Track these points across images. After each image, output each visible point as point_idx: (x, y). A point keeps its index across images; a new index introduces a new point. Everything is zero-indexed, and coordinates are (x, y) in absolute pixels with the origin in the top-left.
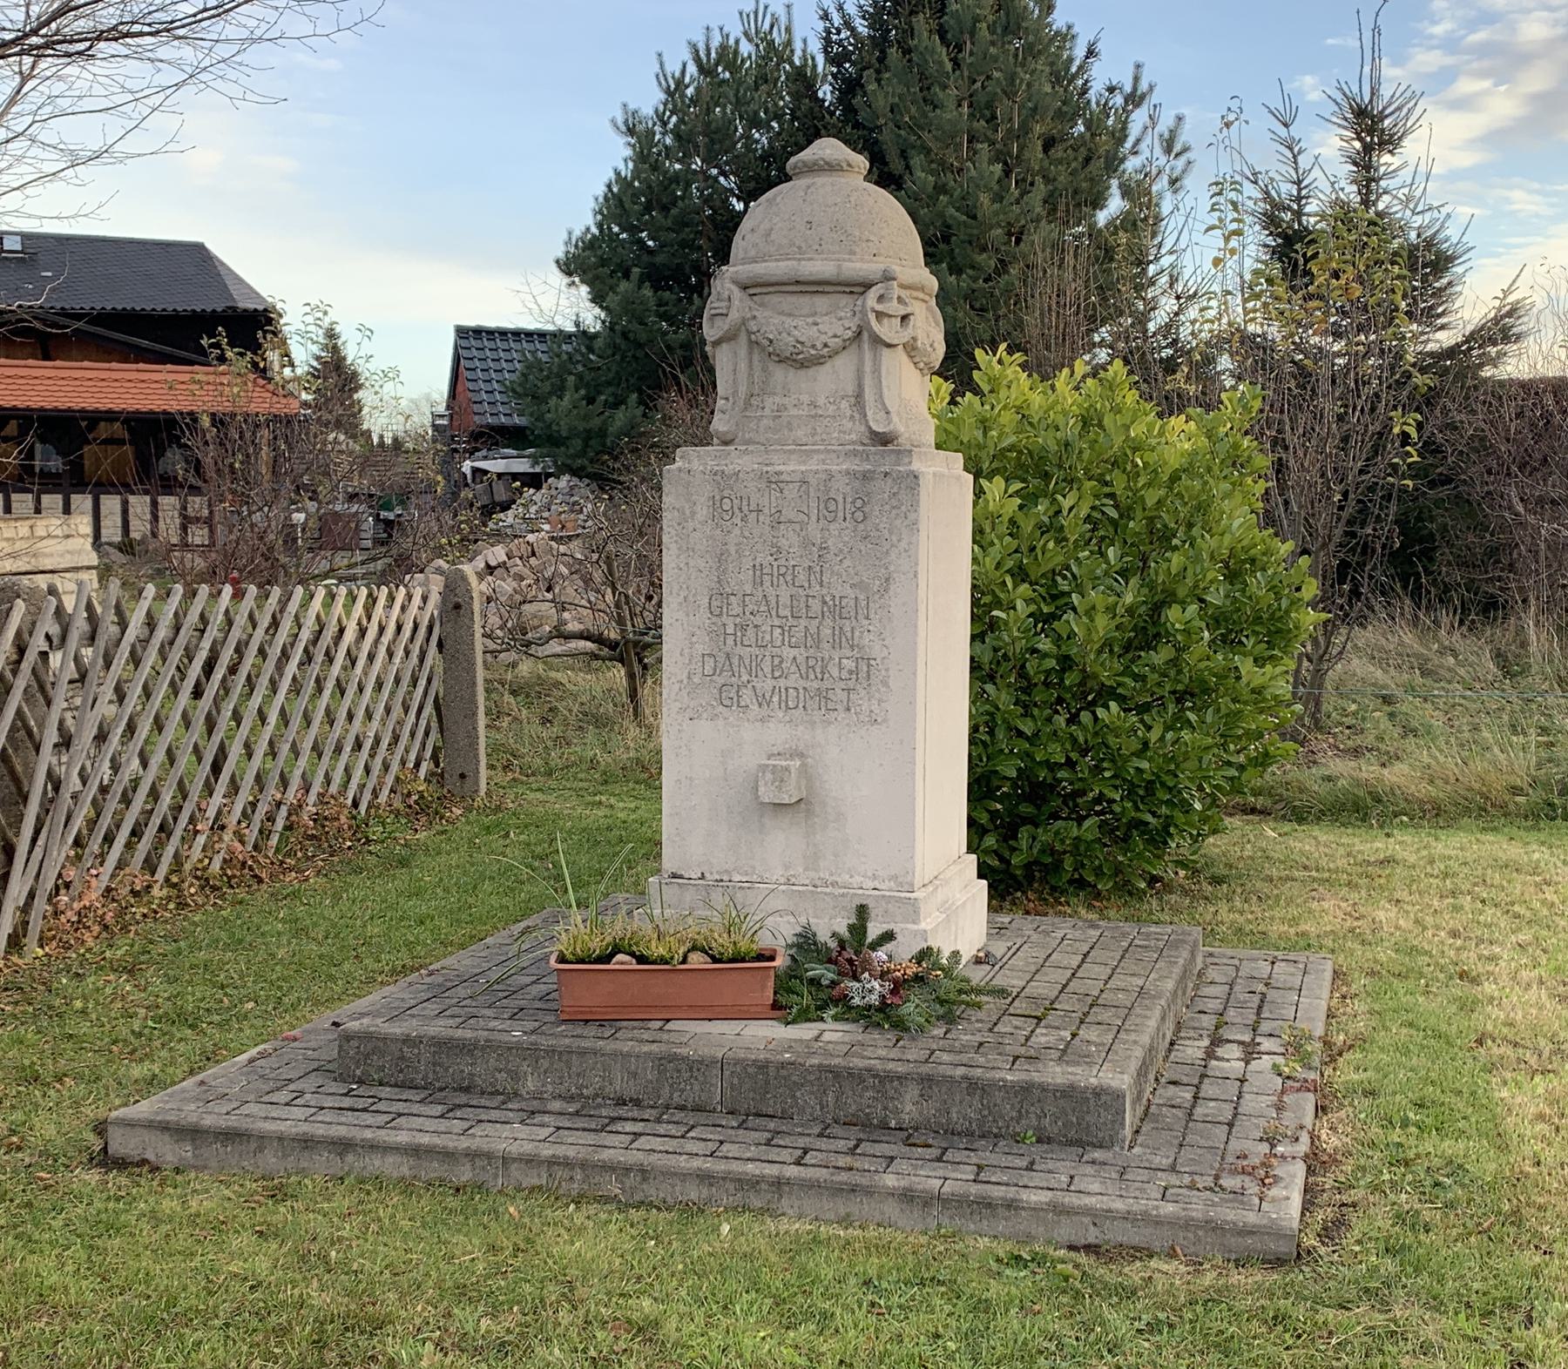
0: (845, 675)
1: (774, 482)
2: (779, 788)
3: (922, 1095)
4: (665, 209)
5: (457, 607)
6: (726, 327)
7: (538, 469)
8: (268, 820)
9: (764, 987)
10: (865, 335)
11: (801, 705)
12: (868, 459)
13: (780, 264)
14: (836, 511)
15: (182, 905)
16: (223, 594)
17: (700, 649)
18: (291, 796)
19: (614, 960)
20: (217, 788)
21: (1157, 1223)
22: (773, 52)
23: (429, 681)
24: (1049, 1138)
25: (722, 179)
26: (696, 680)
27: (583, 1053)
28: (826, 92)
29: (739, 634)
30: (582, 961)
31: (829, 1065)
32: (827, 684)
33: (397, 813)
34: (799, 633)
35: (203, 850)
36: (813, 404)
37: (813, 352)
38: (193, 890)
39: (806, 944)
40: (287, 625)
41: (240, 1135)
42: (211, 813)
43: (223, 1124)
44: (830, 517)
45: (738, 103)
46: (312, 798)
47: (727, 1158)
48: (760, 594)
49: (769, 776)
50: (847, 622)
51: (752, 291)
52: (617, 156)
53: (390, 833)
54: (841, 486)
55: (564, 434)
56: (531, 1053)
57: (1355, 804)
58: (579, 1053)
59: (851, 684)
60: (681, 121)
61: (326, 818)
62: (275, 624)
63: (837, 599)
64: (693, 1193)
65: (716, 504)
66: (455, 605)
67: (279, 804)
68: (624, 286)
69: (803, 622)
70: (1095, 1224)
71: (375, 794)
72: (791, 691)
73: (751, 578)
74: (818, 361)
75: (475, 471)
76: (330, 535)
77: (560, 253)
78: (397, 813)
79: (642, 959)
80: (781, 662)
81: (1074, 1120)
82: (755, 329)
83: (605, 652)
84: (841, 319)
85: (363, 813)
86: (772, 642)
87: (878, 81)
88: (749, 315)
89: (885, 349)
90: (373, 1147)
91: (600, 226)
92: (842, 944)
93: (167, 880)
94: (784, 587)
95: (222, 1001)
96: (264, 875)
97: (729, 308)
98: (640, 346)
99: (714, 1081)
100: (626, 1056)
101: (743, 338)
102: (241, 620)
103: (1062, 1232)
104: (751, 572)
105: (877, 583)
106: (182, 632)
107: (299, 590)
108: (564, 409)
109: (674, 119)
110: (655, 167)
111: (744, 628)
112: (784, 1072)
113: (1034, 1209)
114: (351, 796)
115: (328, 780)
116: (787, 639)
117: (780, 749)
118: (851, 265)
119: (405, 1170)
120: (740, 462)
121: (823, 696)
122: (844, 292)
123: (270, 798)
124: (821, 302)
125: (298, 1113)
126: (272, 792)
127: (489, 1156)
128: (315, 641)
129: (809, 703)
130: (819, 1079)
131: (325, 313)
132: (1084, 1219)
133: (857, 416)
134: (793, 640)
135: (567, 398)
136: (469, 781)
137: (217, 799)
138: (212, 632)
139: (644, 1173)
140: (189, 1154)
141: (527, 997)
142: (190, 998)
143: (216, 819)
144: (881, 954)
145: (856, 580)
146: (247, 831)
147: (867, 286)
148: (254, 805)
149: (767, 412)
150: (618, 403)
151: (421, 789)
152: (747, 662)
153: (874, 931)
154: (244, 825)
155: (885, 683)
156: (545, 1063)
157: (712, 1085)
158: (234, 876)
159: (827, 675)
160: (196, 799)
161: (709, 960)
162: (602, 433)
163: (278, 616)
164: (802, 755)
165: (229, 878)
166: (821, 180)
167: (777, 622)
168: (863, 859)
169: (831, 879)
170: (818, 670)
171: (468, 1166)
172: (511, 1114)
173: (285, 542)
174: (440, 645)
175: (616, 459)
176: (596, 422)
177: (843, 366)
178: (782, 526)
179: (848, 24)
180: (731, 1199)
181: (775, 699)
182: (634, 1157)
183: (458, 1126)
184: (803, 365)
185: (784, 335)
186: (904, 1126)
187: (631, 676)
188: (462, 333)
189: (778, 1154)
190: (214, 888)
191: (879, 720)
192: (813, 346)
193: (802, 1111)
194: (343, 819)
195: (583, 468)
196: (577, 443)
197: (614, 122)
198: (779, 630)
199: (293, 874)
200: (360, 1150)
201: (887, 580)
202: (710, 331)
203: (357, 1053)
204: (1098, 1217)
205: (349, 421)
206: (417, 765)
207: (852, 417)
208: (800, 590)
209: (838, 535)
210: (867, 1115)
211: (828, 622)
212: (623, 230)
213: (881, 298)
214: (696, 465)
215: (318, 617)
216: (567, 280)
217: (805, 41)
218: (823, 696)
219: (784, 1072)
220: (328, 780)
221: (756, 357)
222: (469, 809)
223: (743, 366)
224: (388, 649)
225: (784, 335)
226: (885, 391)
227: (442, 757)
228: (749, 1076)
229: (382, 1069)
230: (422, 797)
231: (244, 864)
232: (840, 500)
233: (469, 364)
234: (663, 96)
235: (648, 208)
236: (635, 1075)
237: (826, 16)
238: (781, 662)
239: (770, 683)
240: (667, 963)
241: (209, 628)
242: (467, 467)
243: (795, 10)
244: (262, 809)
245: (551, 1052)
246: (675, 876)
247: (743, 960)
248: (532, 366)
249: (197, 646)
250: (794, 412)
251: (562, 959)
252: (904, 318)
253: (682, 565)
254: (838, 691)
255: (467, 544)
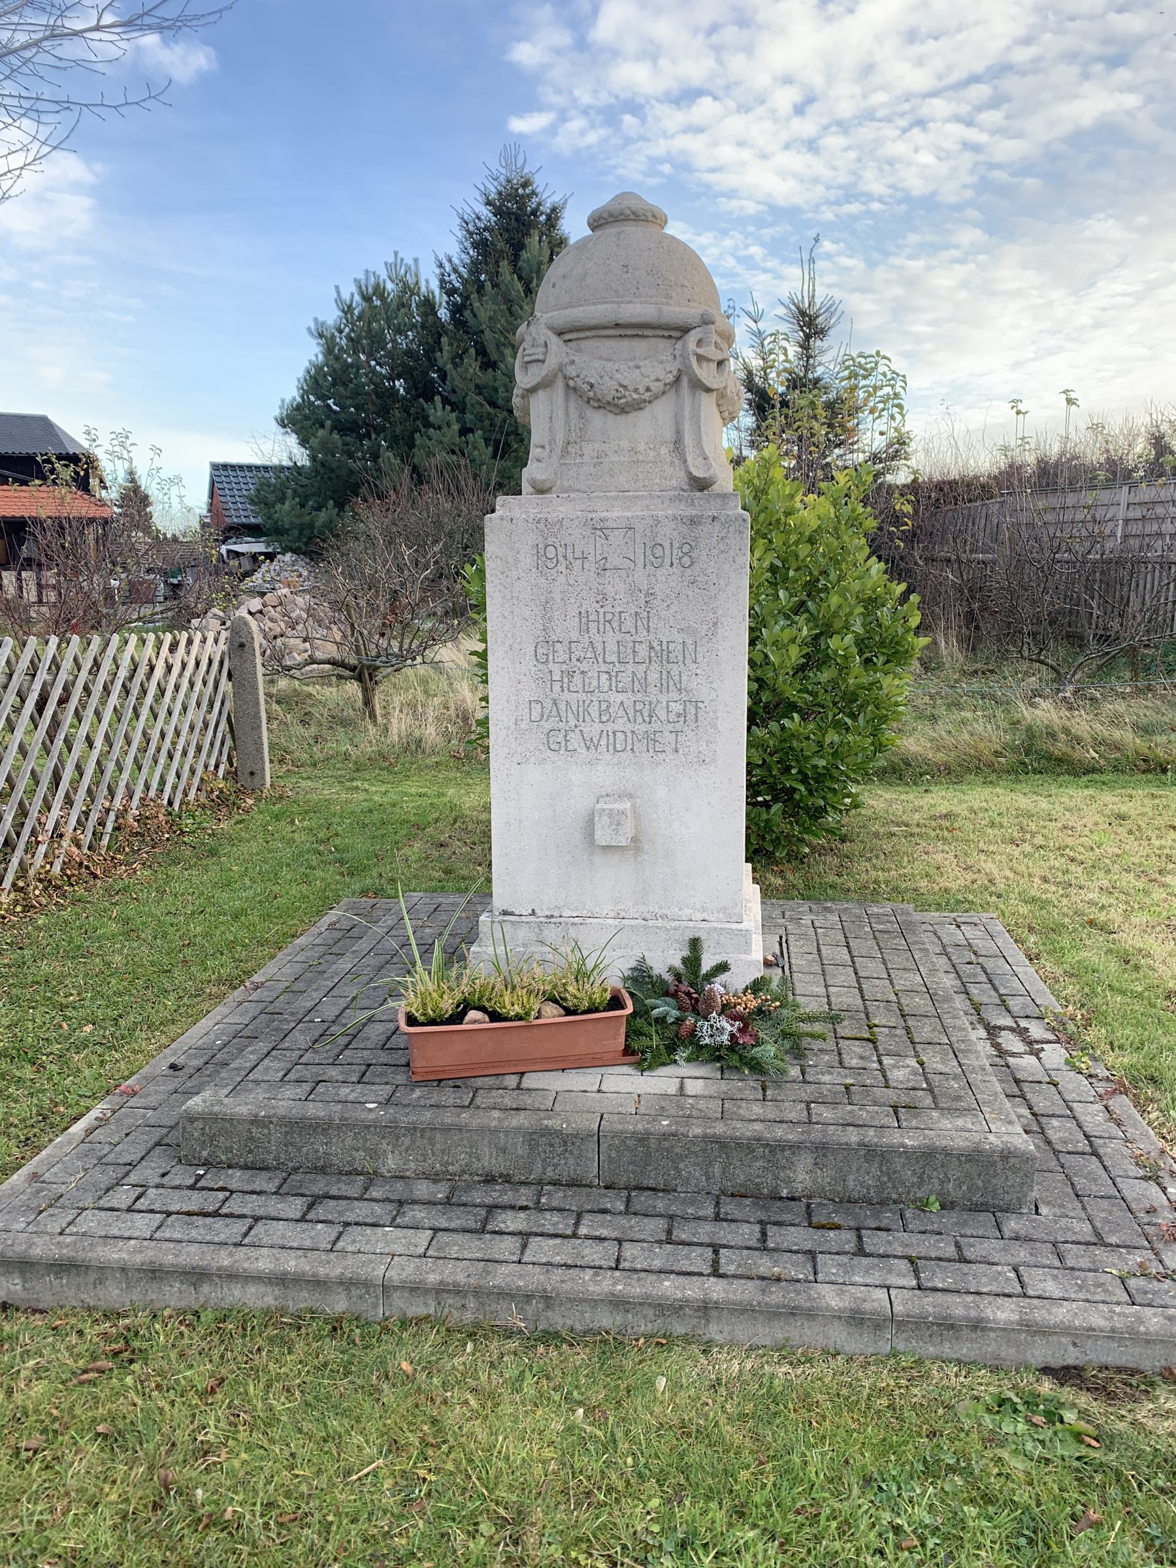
0: (672, 717)
1: (600, 529)
2: (616, 831)
3: (816, 1164)
4: (345, 385)
5: (242, 645)
6: (544, 373)
7: (270, 550)
8: (99, 824)
9: (615, 1037)
10: (685, 380)
11: (629, 748)
12: (693, 504)
13: (599, 307)
14: (663, 557)
15: (27, 908)
16: (50, 643)
17: (527, 695)
18: (118, 804)
19: (467, 1018)
20: (54, 804)
21: (1148, 1342)
22: (408, 289)
23: (223, 703)
24: (952, 1203)
25: (378, 368)
26: (523, 726)
27: (447, 1130)
28: (443, 314)
29: (566, 680)
30: (432, 1022)
31: (714, 1136)
32: (656, 726)
33: (204, 807)
34: (626, 679)
35: (46, 856)
36: (634, 451)
37: (635, 396)
38: (37, 892)
39: (641, 977)
40: (107, 666)
41: (77, 1267)
42: (50, 826)
43: (56, 1253)
44: (657, 562)
45: (388, 320)
46: (135, 802)
47: (635, 1270)
48: (587, 641)
49: (605, 820)
50: (675, 667)
51: (567, 337)
52: (311, 353)
53: (200, 823)
54: (668, 533)
55: (287, 526)
56: (391, 1131)
57: (894, 768)
58: (443, 1130)
59: (678, 727)
60: (352, 330)
61: (147, 818)
62: (97, 664)
63: (665, 643)
64: (606, 1319)
65: (540, 552)
66: (240, 646)
67: (108, 811)
68: (321, 432)
69: (630, 668)
70: (1075, 1344)
71: (186, 794)
72: (619, 734)
73: (577, 625)
74: (637, 406)
75: (229, 551)
76: (136, 594)
77: (277, 412)
78: (204, 807)
79: (495, 1016)
80: (608, 707)
81: (980, 1184)
82: (574, 374)
83: (347, 673)
84: (662, 363)
85: (177, 809)
86: (599, 687)
87: (480, 301)
88: (566, 360)
89: (704, 394)
90: (231, 1276)
91: (302, 397)
92: (678, 977)
93: (14, 885)
94: (611, 633)
95: (61, 1027)
96: (98, 872)
97: (545, 354)
98: (332, 470)
99: (590, 1155)
100: (494, 1131)
101: (560, 384)
102: (67, 664)
103: (1037, 1353)
104: (577, 619)
105: (705, 627)
106: (15, 676)
107: (116, 638)
108: (286, 510)
109: (347, 329)
110: (337, 358)
111: (571, 674)
112: (666, 1144)
113: (1005, 1329)
114: (166, 796)
115: (147, 787)
116: (614, 685)
117: (610, 791)
118: (672, 308)
119: (270, 1301)
120: (562, 509)
121: (651, 739)
122: (663, 337)
123: (100, 807)
124: (640, 346)
125: (142, 1224)
126: (102, 802)
127: (367, 1284)
128: (131, 678)
129: (637, 745)
130: (704, 1150)
131: (127, 437)
132: (1063, 1340)
133: (677, 462)
134: (620, 685)
135: (287, 503)
136: (257, 778)
137: (55, 813)
138: (42, 676)
139: (548, 1300)
140: (18, 1287)
141: (369, 1044)
142: (30, 1025)
143: (55, 829)
144: (717, 986)
145: (684, 625)
146: (82, 837)
147: (685, 330)
148: (86, 814)
149: (586, 458)
150: (318, 508)
151: (221, 786)
152: (574, 708)
153: (706, 965)
154: (79, 832)
155: (713, 725)
156: (407, 1141)
157: (588, 1159)
158: (73, 875)
159: (655, 718)
160: (36, 815)
161: (562, 1012)
162: (311, 526)
163: (99, 659)
164: (630, 796)
165: (69, 877)
166: (630, 229)
167: (604, 668)
168: (692, 893)
169: (660, 912)
170: (646, 714)
171: (343, 1295)
172: (377, 1208)
173: (106, 599)
174: (230, 676)
175: (324, 541)
176: (307, 519)
177: (660, 415)
178: (608, 573)
179: (455, 270)
180: (649, 1325)
181: (603, 742)
182: (531, 1279)
183: (323, 1234)
184: (623, 410)
185: (606, 378)
186: (797, 1194)
187: (365, 690)
188: (215, 467)
189: (688, 1257)
190: (57, 887)
191: (707, 760)
192: (636, 390)
193: (687, 1182)
194: (161, 817)
195: (299, 548)
196: (296, 532)
197: (309, 329)
198: (607, 676)
199: (123, 867)
200: (217, 1280)
201: (715, 624)
202: (523, 379)
203: (203, 1135)
204: (1080, 1335)
205: (143, 522)
206: (217, 767)
207: (672, 463)
208: (627, 636)
209: (666, 580)
210: (757, 1184)
211: (655, 666)
212: (318, 398)
213: (700, 343)
214: (517, 513)
215: (132, 658)
216: (283, 430)
217: (427, 281)
218: (651, 739)
219: (666, 1144)
220: (147, 787)
221: (572, 404)
222: (258, 800)
223: (560, 412)
224: (190, 681)
225: (606, 378)
226: (704, 436)
227: (234, 760)
228: (628, 1148)
229: (229, 1150)
230: (221, 792)
231: (81, 864)
232: (667, 545)
233: (220, 486)
234: (341, 314)
235: (334, 384)
236: (504, 1151)
237: (441, 266)
238: (608, 707)
239: (598, 727)
240: (521, 1019)
241: (39, 672)
242: (224, 549)
243: (420, 262)
244: (94, 817)
245: (412, 1129)
246: (505, 913)
247: (597, 1010)
248: (264, 485)
249: (29, 689)
250: (615, 458)
251: (411, 1021)
252: (720, 363)
253: (506, 614)
254: (666, 733)
255: (231, 598)
